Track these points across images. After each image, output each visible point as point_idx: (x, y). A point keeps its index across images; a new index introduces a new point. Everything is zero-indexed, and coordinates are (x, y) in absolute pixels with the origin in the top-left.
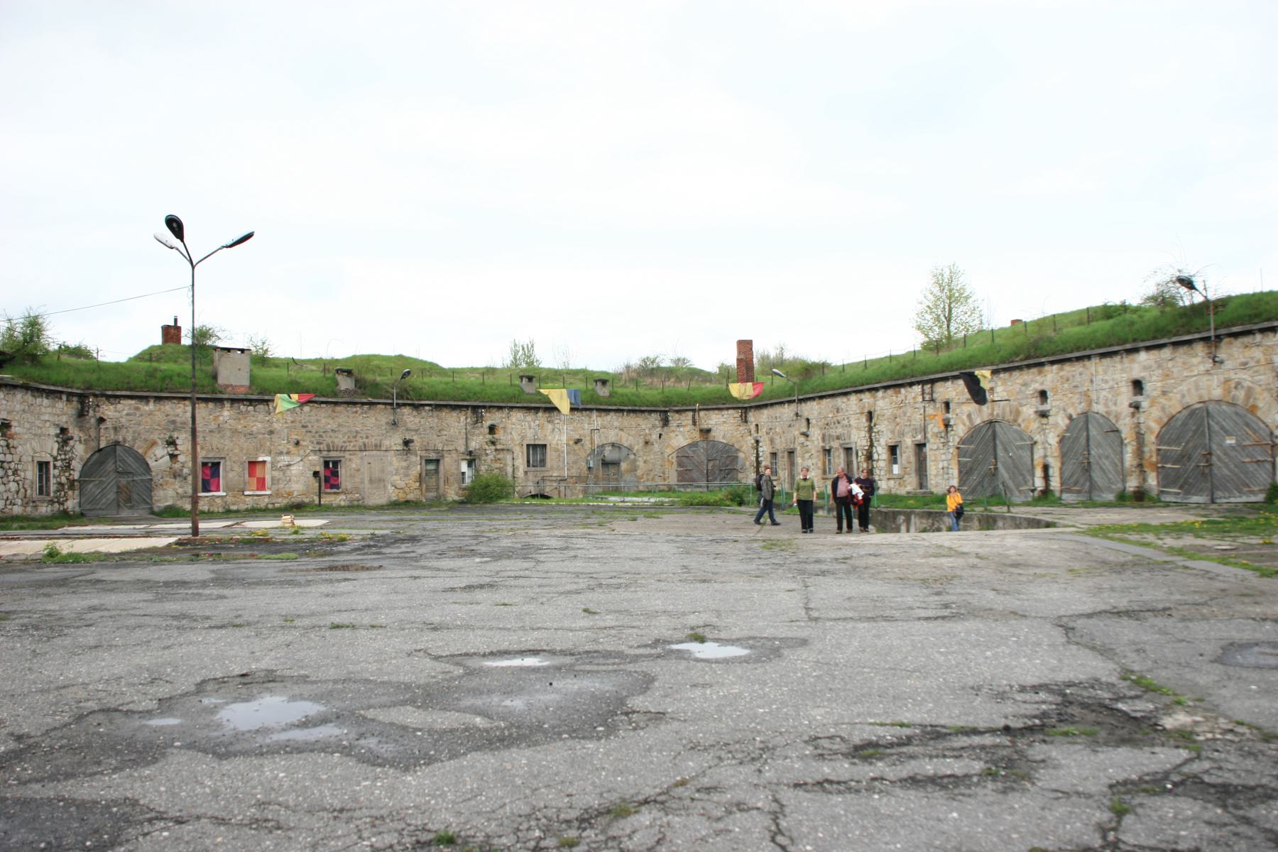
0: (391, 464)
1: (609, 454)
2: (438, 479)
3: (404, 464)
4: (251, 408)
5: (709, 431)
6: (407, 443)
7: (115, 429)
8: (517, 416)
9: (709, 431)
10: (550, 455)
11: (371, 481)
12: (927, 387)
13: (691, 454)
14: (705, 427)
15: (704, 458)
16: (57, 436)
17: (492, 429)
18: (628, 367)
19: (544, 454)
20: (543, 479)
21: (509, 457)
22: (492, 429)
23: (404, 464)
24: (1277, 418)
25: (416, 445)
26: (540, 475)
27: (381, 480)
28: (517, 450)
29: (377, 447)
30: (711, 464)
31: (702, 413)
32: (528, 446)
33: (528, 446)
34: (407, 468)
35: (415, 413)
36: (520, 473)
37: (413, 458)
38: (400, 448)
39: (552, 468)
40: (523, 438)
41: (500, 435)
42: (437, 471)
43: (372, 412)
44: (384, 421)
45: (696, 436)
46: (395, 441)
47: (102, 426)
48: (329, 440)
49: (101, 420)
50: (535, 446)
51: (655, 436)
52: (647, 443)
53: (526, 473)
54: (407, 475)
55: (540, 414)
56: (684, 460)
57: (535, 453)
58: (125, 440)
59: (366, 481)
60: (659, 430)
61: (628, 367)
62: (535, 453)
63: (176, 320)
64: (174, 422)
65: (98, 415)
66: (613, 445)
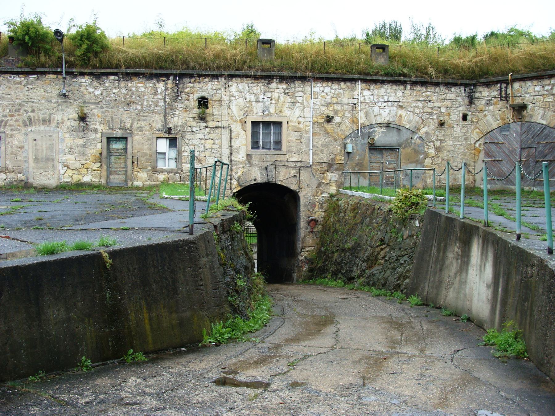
0: (63, 141)
1: (380, 137)
2: (126, 162)
3: (81, 142)
5: (523, 107)
6: (83, 118)
8: (237, 87)
9: (523, 107)
10: (287, 135)
11: (36, 160)
12: (116, 179)
13: (501, 140)
14: (519, 101)
15: (516, 146)
17: (203, 103)
18: (467, 37)
19: (279, 134)
20: (275, 165)
21: (225, 134)
22: (203, 103)
23: (81, 142)
24: (554, 263)
25: (411, 136)
26: (270, 159)
27: (48, 159)
28: (236, 127)
29: (46, 121)
30: (525, 154)
31: (516, 85)
32: (255, 124)
33: (255, 124)
34: (84, 146)
35: (95, 83)
36: (240, 157)
37: (92, 135)
38: (75, 124)
39: (289, 152)
40: (246, 114)
41: (213, 109)
43: (40, 83)
44: (55, 92)
45: (509, 116)
46: (70, 113)
50: (267, 124)
51: (456, 116)
52: (442, 124)
53: (249, 156)
54: (83, 155)
55: (273, 85)
56: (493, 147)
57: (267, 134)
59: (31, 160)
60: (463, 109)
61: (467, 37)
62: (267, 134)
66: (388, 125)
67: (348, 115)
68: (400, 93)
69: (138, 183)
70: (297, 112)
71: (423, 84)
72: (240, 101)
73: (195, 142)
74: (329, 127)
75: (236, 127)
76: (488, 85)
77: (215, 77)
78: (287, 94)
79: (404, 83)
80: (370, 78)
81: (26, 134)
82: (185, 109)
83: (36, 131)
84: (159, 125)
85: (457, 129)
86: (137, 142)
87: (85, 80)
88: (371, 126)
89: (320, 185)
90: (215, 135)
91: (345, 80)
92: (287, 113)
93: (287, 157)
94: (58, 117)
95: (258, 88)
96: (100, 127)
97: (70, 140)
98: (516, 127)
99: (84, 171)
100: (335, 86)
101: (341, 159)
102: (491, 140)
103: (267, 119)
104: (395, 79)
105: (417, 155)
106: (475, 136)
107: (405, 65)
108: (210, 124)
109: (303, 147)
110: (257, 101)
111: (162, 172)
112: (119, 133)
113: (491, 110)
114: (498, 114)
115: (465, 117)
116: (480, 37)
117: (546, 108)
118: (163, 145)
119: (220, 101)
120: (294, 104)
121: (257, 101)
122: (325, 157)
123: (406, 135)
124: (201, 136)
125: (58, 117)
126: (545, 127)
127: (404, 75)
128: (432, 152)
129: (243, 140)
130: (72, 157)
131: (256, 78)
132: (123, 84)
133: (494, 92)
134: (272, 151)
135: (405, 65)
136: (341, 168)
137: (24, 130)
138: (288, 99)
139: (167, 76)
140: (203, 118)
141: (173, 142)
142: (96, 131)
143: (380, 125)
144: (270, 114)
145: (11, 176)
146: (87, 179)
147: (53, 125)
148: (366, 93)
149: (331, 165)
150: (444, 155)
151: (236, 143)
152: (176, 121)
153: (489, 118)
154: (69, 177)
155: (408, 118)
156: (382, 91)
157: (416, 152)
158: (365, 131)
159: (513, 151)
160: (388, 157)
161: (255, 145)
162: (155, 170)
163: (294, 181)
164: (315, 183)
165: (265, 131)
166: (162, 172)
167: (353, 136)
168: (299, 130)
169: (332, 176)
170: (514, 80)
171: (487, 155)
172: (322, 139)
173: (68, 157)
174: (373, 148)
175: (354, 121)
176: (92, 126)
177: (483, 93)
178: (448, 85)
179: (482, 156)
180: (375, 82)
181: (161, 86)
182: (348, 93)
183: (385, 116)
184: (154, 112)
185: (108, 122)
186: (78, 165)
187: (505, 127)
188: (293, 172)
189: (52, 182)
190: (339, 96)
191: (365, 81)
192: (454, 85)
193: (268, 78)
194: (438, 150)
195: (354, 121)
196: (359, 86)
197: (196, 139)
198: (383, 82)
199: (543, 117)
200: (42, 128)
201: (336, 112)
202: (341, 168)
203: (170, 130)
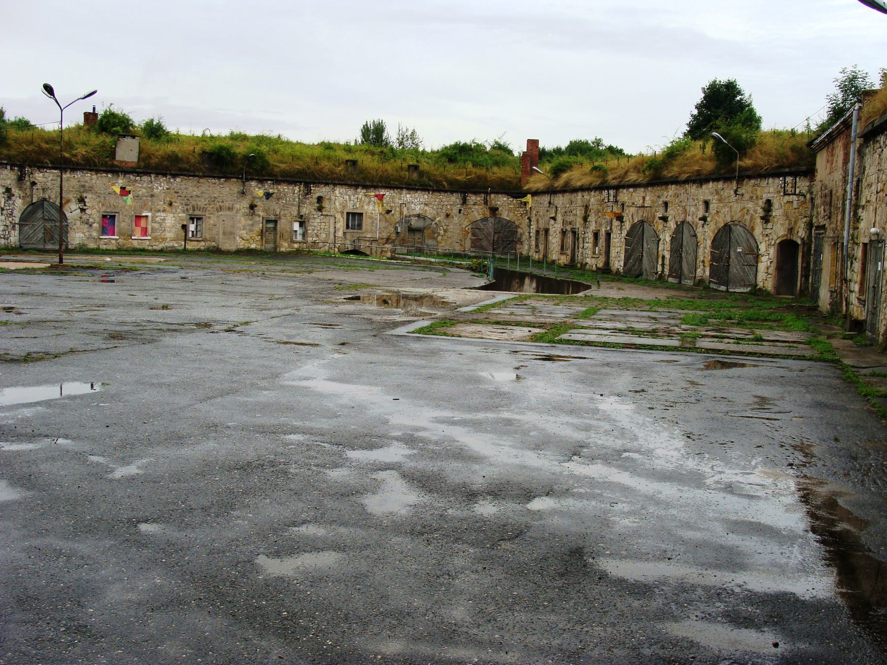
0: (240, 221)
1: (415, 223)
3: (250, 222)
4: (138, 178)
7: (43, 189)
8: (338, 190)
10: (366, 222)
11: (224, 233)
15: (491, 230)
16: (4, 193)
17: (320, 199)
20: (359, 239)
21: (332, 220)
22: (320, 199)
23: (250, 222)
26: (356, 236)
27: (231, 233)
28: (338, 216)
30: (496, 236)
31: (493, 196)
32: (348, 214)
33: (348, 214)
34: (252, 225)
35: (260, 186)
36: (340, 234)
37: (257, 219)
38: (247, 211)
41: (326, 204)
42: (275, 228)
43: (227, 184)
45: (488, 214)
46: (245, 204)
47: (35, 188)
48: (194, 203)
49: (34, 184)
50: (354, 214)
52: (448, 216)
54: (251, 231)
55: (359, 190)
56: (477, 231)
58: (50, 197)
63: (94, 109)
64: (83, 186)
65: (32, 180)
66: (419, 216)
67: (398, 209)
68: (426, 197)
69: (283, 249)
70: (371, 207)
71: (439, 191)
72: (342, 199)
73: (315, 224)
74: (387, 216)
75: (338, 216)
76: (475, 193)
77: (327, 184)
78: (366, 196)
79: (428, 191)
80: (411, 187)
81: (218, 217)
82: (311, 203)
83: (224, 215)
84: (295, 213)
85: (456, 218)
86: (282, 224)
87: (253, 183)
88: (410, 216)
89: (382, 252)
90: (326, 220)
91: (397, 188)
92: (366, 207)
93: (365, 235)
94: (237, 206)
95: (351, 192)
96: (261, 214)
97: (243, 221)
98: (491, 220)
99: (251, 241)
100: (392, 191)
101: (393, 236)
102: (476, 229)
103: (355, 211)
104: (424, 187)
105: (434, 235)
106: (466, 223)
107: (430, 180)
108: (324, 213)
109: (374, 228)
110: (350, 200)
111: (296, 242)
112: (272, 217)
113: (477, 208)
114: (481, 211)
115: (460, 211)
116: (589, 142)
117: (510, 210)
118: (296, 226)
119: (330, 199)
120: (369, 202)
121: (350, 200)
122: (385, 235)
123: (428, 222)
124: (318, 220)
125: (237, 206)
126: (509, 221)
127: (430, 186)
128: (442, 232)
129: (341, 224)
130: (245, 232)
131: (350, 186)
132: (275, 187)
133: (479, 198)
134: (356, 231)
135: (430, 180)
136: (393, 242)
137: (217, 214)
138: (367, 200)
139: (300, 183)
140: (320, 209)
141: (302, 224)
142: (259, 216)
143: (415, 216)
144: (357, 208)
145: (208, 244)
146: (253, 246)
147: (234, 211)
148: (408, 196)
149: (388, 240)
150: (449, 234)
151: (338, 226)
152: (304, 211)
153: (475, 213)
154: (241, 244)
155: (430, 212)
156: (417, 195)
157: (434, 232)
158: (406, 220)
159: (489, 234)
160: (418, 236)
161: (348, 227)
162: (293, 242)
163: (369, 249)
164: (379, 251)
165: (355, 219)
166: (296, 242)
167: (400, 222)
168: (372, 218)
169: (389, 246)
170: (491, 193)
171: (473, 235)
172: (384, 224)
173: (243, 232)
174: (411, 230)
175: (401, 213)
176: (257, 213)
177: (472, 198)
178: (452, 192)
179: (470, 235)
180: (413, 189)
181: (297, 188)
182: (398, 196)
183: (418, 209)
184: (293, 205)
185: (266, 210)
186: (248, 237)
187: (485, 220)
188: (368, 244)
189: (233, 248)
190: (393, 197)
191: (408, 189)
192: (456, 192)
193: (356, 186)
194: (445, 231)
195: (401, 213)
196: (404, 191)
197: (316, 223)
198: (417, 190)
199: (508, 216)
200: (228, 213)
201: (392, 207)
202: (393, 242)
203: (302, 216)
